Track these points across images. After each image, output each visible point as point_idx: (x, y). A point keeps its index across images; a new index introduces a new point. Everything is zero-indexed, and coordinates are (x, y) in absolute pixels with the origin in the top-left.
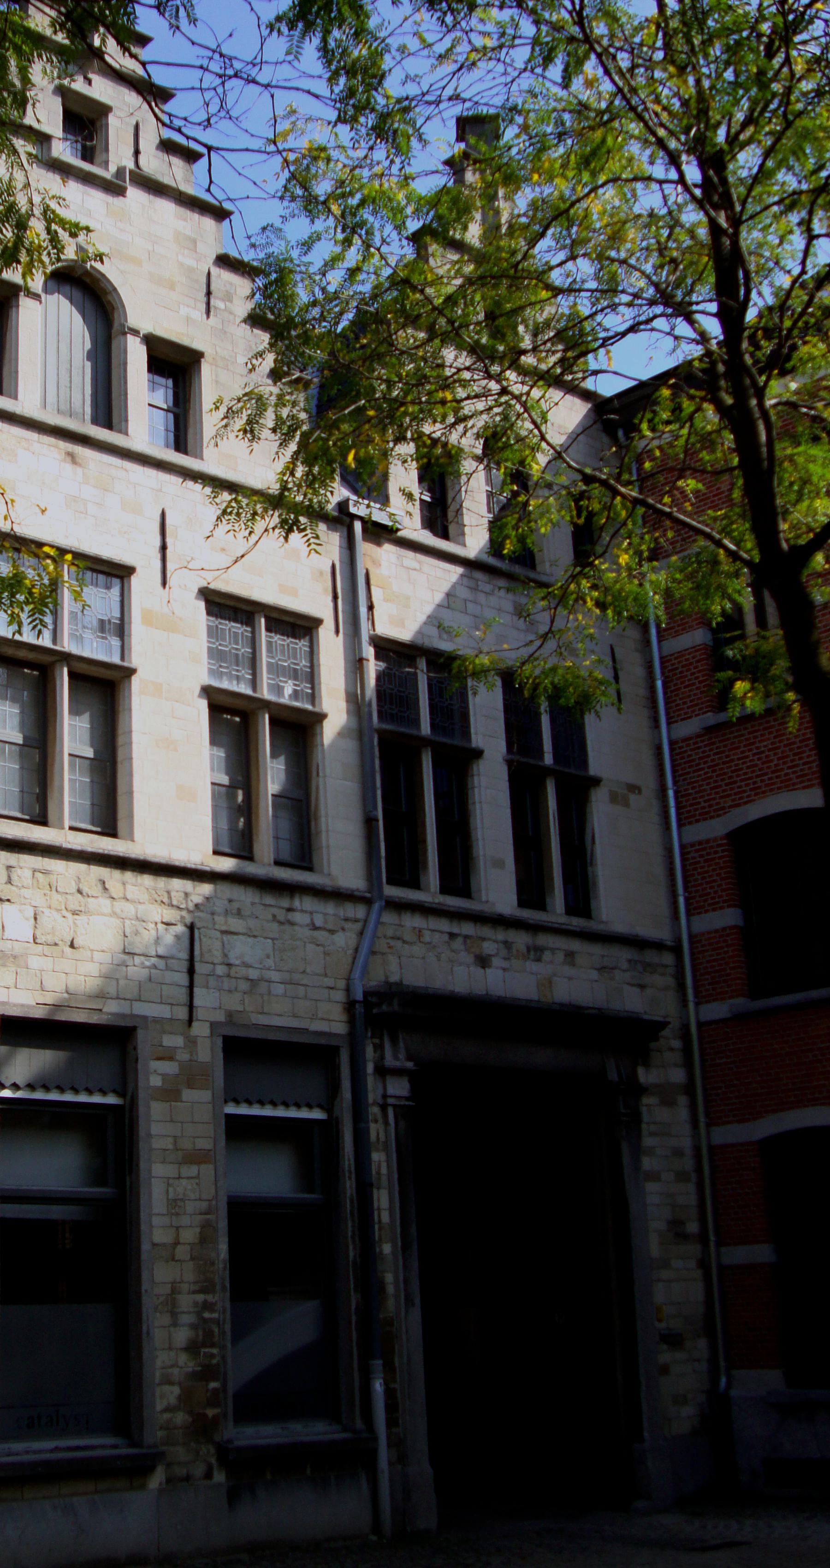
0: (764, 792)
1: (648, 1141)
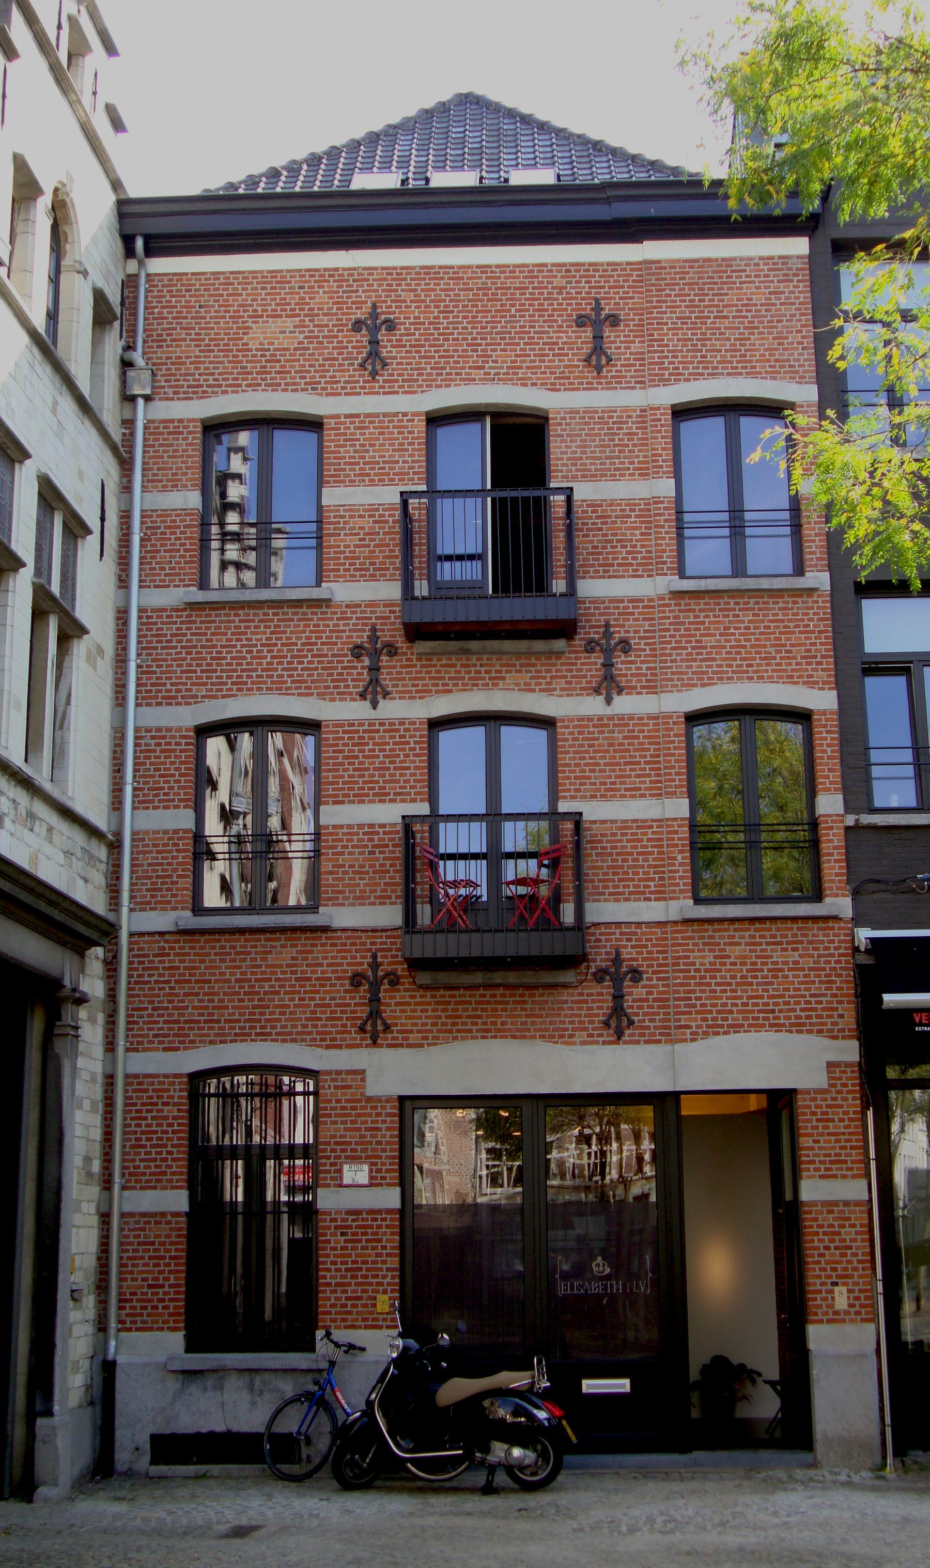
0: (249, 689)
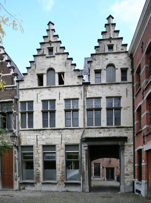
1: (125, 151)
